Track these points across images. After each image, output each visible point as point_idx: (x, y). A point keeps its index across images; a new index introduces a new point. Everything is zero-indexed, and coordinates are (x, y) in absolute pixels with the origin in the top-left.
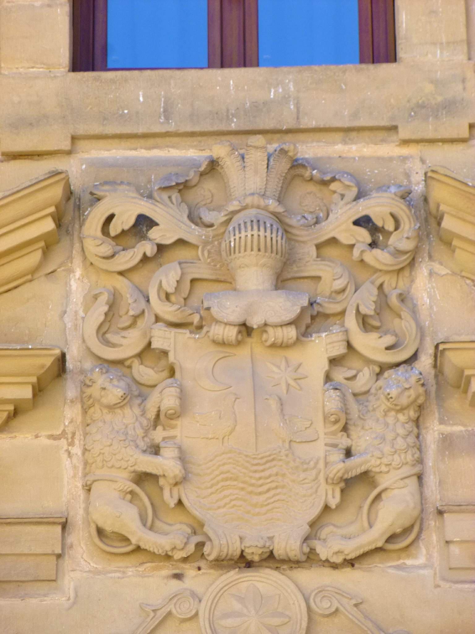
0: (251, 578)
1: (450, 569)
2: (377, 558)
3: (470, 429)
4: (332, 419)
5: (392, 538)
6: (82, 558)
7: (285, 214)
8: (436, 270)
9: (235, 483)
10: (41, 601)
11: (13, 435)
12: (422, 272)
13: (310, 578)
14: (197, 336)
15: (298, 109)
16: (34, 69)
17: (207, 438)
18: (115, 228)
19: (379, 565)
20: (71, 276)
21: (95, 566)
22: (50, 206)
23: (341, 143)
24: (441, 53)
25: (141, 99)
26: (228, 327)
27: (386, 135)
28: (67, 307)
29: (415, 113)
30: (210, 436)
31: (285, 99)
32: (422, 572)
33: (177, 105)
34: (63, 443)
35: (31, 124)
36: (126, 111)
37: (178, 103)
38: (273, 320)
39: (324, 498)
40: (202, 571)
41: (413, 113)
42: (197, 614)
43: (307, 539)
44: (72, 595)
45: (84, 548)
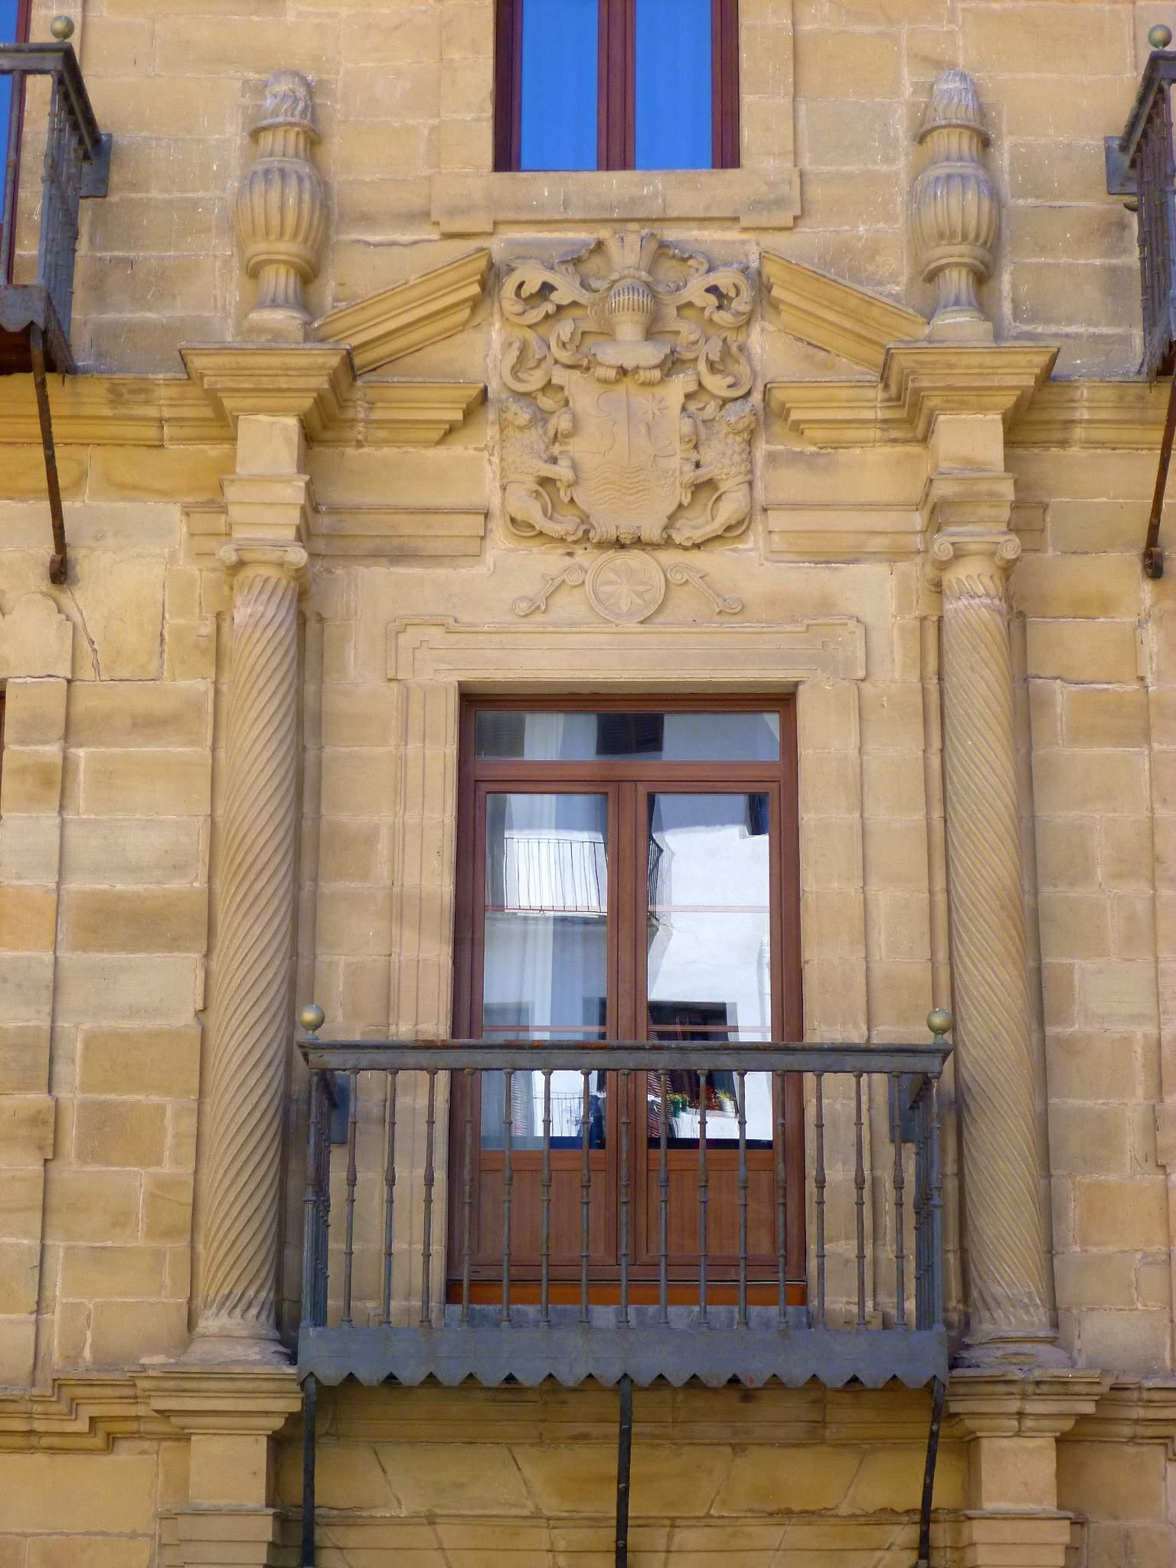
2: (716, 543)
5: (729, 528)
18: (526, 292)
31: (655, 195)
34: (486, 454)
38: (642, 364)
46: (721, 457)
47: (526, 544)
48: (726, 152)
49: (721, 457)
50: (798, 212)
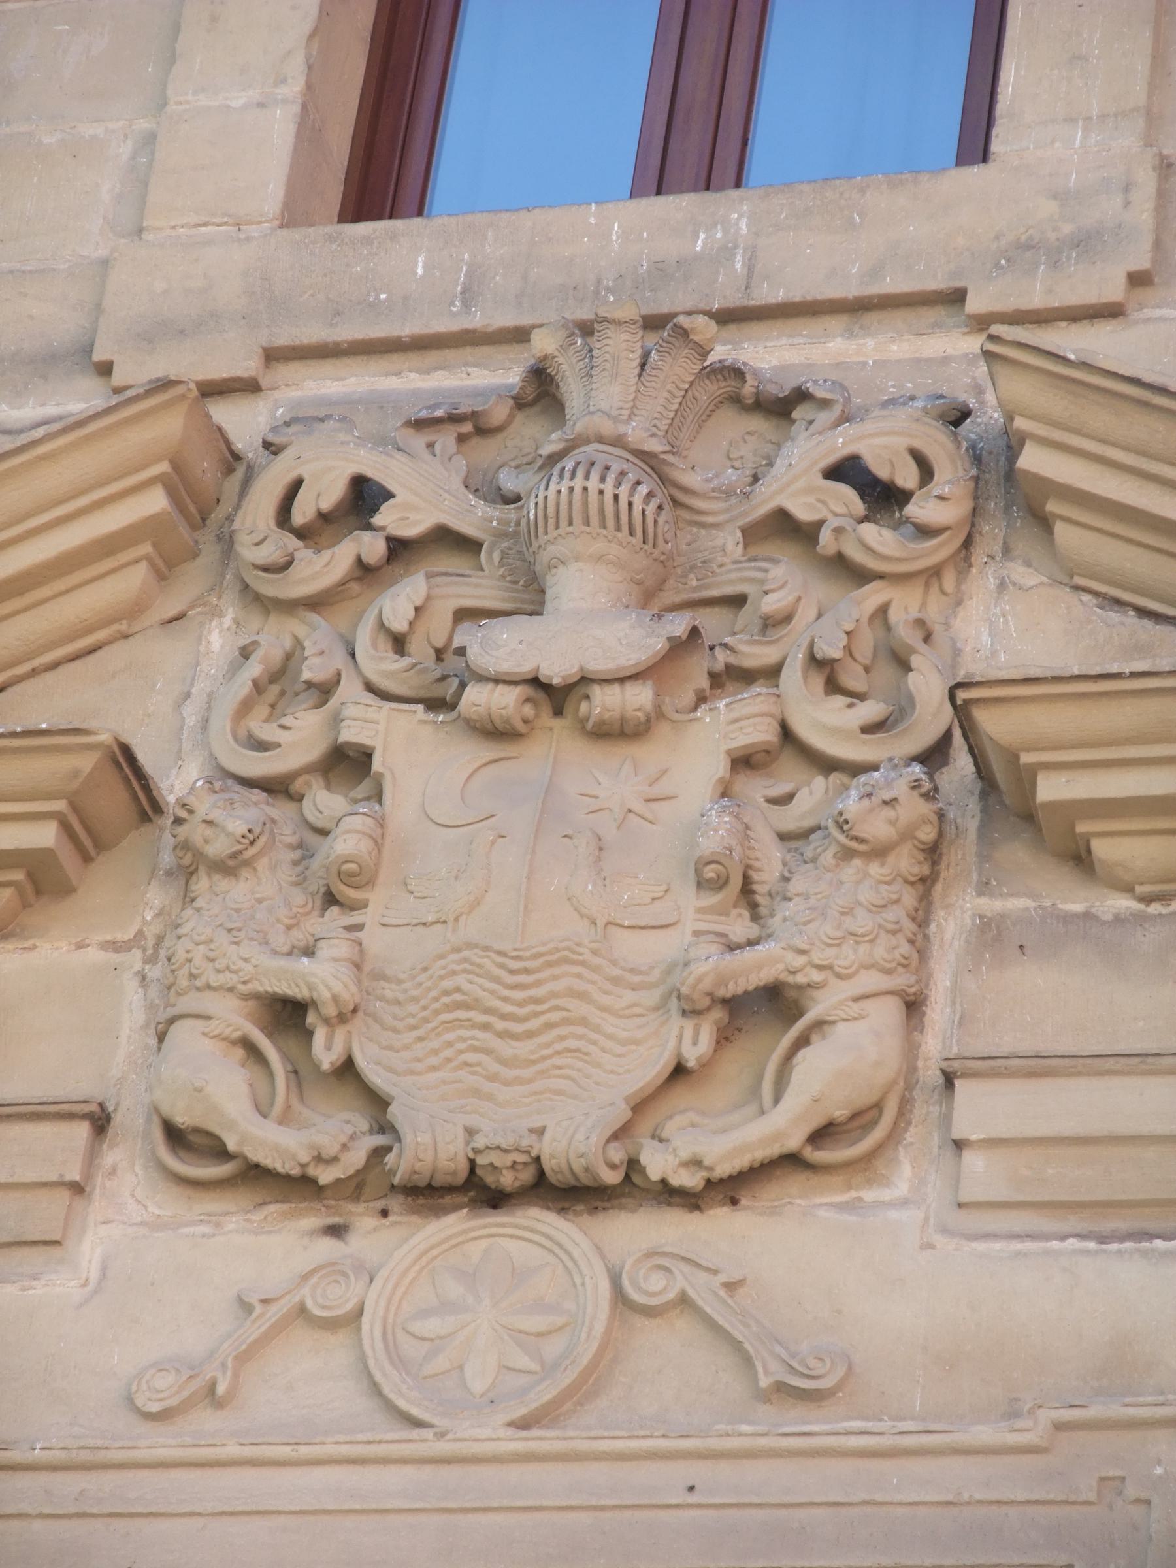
0: (494, 1230)
1: (960, 1205)
2: (793, 1185)
3: (1047, 903)
4: (710, 872)
5: (822, 1135)
6: (133, 1196)
7: (670, 458)
8: (1016, 577)
9: (472, 1014)
10: (24, 1289)
11: (28, 944)
12: (983, 581)
13: (633, 1231)
14: (441, 717)
15: (750, 270)
16: (209, 228)
17: (424, 924)
18: (302, 514)
19: (798, 1201)
20: (214, 623)
21: (157, 1212)
22: (158, 460)
23: (842, 336)
24: (1085, 137)
25: (420, 271)
26: (500, 686)
27: (943, 313)
28: (192, 685)
29: (1008, 260)
30: (430, 919)
31: (726, 251)
32: (893, 1214)
33: (494, 278)
34: (135, 958)
35: (182, 332)
36: (383, 296)
37: (496, 274)
38: (598, 664)
39: (672, 1044)
40: (391, 1218)
41: (1003, 262)
42: (360, 1312)
43: (619, 1134)
44: (94, 1275)
45: (140, 1173)
46: (828, 926)
47: (212, 1204)
48: (975, 144)
49: (828, 926)
50: (1141, 261)
